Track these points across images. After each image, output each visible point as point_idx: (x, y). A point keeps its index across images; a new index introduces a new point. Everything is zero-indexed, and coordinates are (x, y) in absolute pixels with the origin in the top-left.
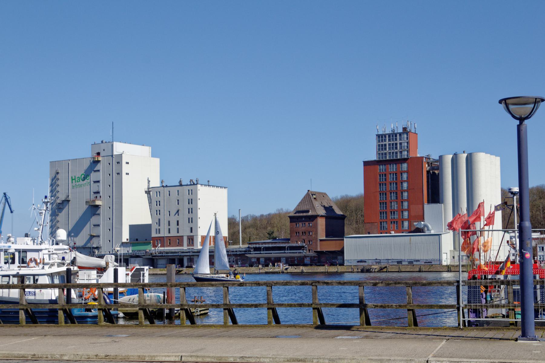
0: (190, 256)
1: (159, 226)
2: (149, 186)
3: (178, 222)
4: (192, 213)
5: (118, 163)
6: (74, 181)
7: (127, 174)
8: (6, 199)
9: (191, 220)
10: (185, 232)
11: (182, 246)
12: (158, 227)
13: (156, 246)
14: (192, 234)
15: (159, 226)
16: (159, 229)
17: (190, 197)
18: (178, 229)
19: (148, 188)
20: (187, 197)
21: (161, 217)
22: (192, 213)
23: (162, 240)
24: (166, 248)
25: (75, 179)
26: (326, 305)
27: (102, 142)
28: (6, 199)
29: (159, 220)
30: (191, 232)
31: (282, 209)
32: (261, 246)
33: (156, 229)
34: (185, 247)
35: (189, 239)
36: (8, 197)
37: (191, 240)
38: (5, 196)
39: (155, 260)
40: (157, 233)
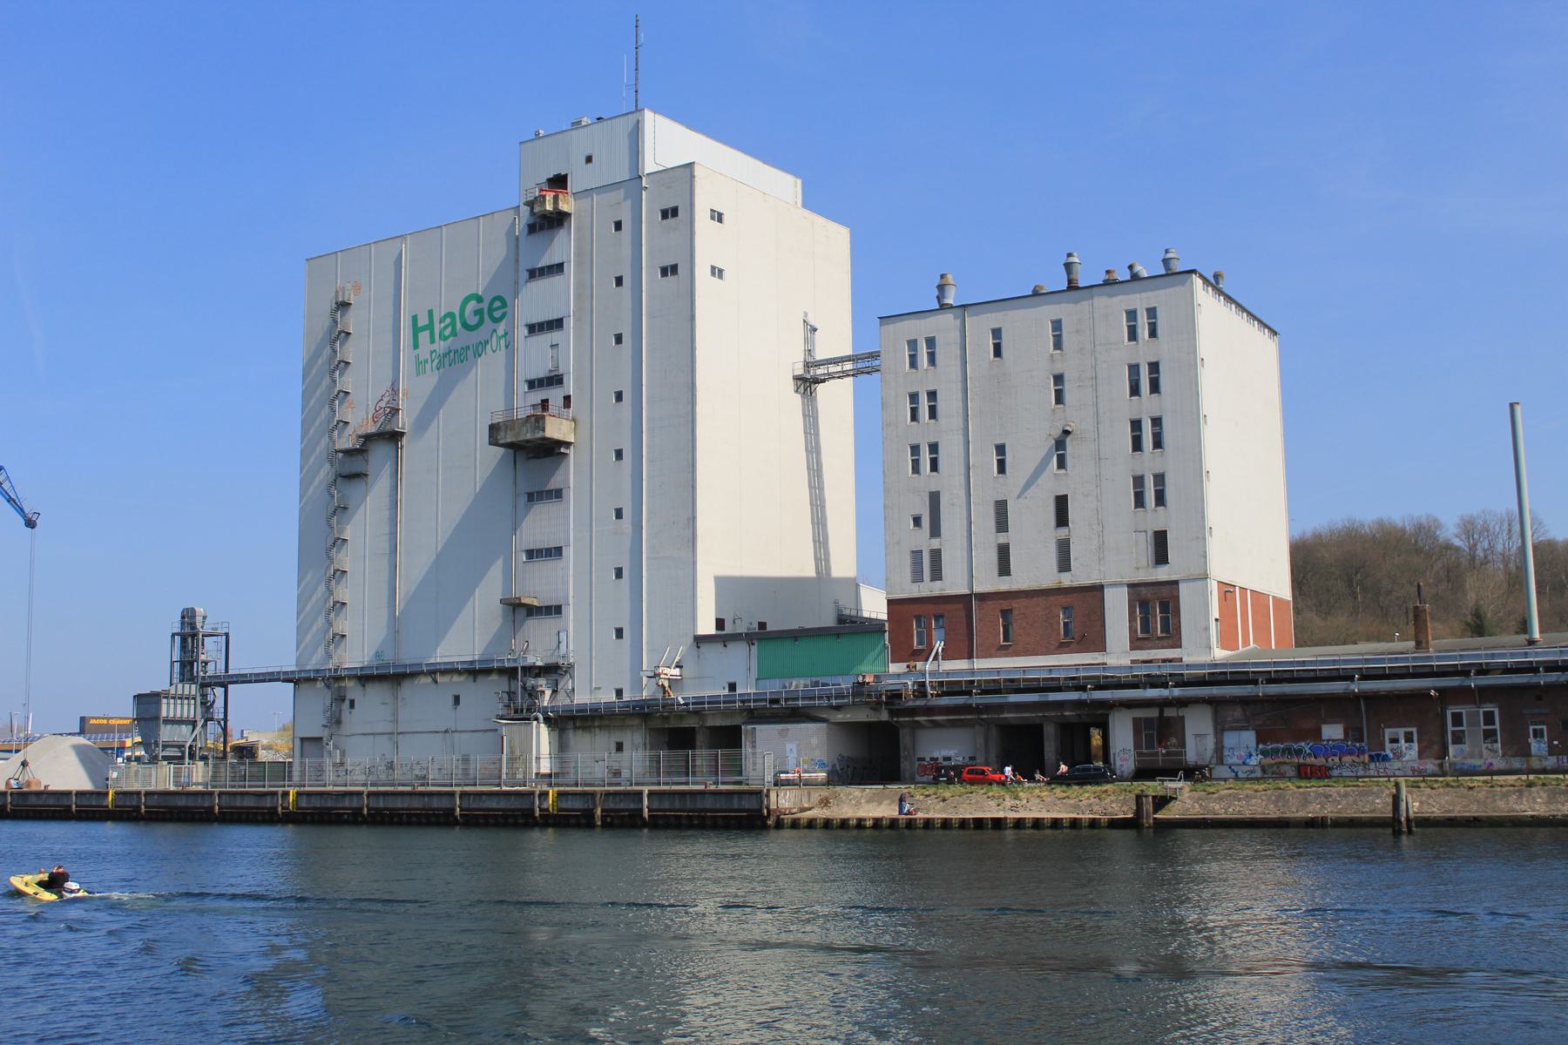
6: (424, 337)
13: (923, 655)
14: (1162, 574)
15: (935, 531)
16: (936, 555)
34: (1118, 654)
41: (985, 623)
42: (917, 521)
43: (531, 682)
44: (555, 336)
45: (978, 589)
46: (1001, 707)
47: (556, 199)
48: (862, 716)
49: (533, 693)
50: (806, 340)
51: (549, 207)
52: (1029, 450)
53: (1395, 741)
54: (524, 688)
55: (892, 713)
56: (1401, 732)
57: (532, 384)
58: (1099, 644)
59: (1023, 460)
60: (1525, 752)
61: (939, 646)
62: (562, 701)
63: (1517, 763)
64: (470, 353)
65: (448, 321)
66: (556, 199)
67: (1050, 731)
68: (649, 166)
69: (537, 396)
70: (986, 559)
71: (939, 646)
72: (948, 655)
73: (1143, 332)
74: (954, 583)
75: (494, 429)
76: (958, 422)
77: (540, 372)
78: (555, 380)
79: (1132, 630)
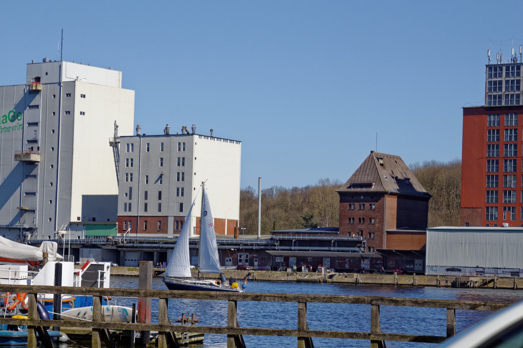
14: (181, 214)
15: (130, 198)
16: (130, 204)
41: (141, 224)
42: (126, 194)
43: (24, 233)
44: (35, 128)
45: (139, 215)
46: (143, 247)
47: (36, 86)
48: (110, 247)
49: (25, 236)
50: (115, 129)
51: (34, 88)
52: (153, 178)
53: (227, 261)
54: (23, 235)
55: (117, 247)
56: (228, 259)
57: (29, 141)
58: (166, 232)
59: (152, 180)
60: (253, 265)
61: (129, 229)
62: (33, 238)
63: (252, 268)
64: (11, 129)
65: (5, 118)
66: (36, 86)
67: (155, 254)
68: (64, 79)
69: (30, 146)
70: (142, 207)
71: (129, 229)
72: (131, 232)
73: (182, 149)
74: (133, 213)
75: (16, 156)
76: (137, 168)
77: (31, 139)
78: (35, 141)
79: (174, 229)
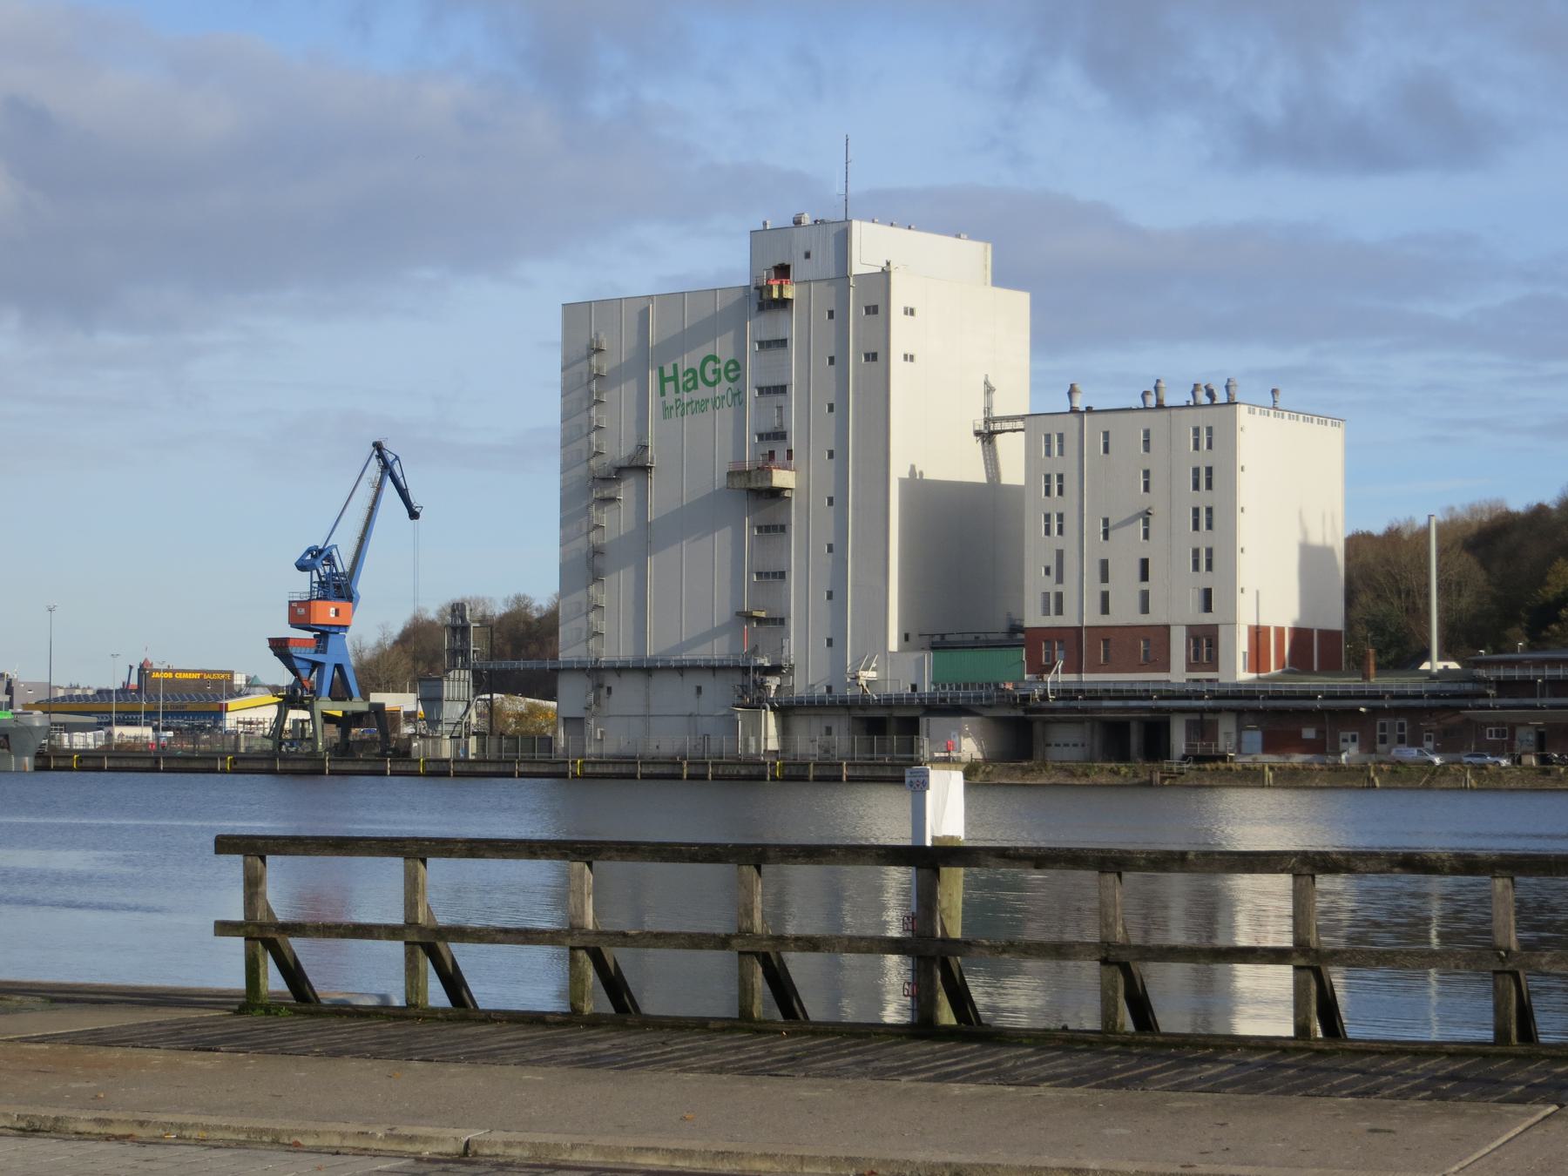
0: (1201, 711)
1: (1060, 580)
2: (988, 409)
3: (1145, 563)
4: (1209, 526)
5: (872, 310)
6: (670, 386)
7: (909, 358)
8: (386, 468)
9: (1205, 560)
10: (1176, 609)
11: (1166, 667)
12: (1050, 585)
13: (1048, 669)
14: (1207, 619)
15: (1060, 580)
16: (1059, 596)
17: (1203, 459)
18: (1145, 595)
19: (987, 421)
20: (1189, 458)
21: (1069, 543)
22: (1209, 526)
23: (1073, 644)
24: (1085, 677)
25: (675, 378)
26: (810, 944)
27: (797, 222)
28: (386, 468)
29: (1060, 554)
30: (1208, 608)
31: (1452, 509)
32: (1531, 673)
33: (1047, 595)
34: (1178, 674)
35: (1197, 643)
36: (390, 458)
37: (1206, 643)
38: (381, 456)
39: (1037, 728)
40: (1046, 612)
